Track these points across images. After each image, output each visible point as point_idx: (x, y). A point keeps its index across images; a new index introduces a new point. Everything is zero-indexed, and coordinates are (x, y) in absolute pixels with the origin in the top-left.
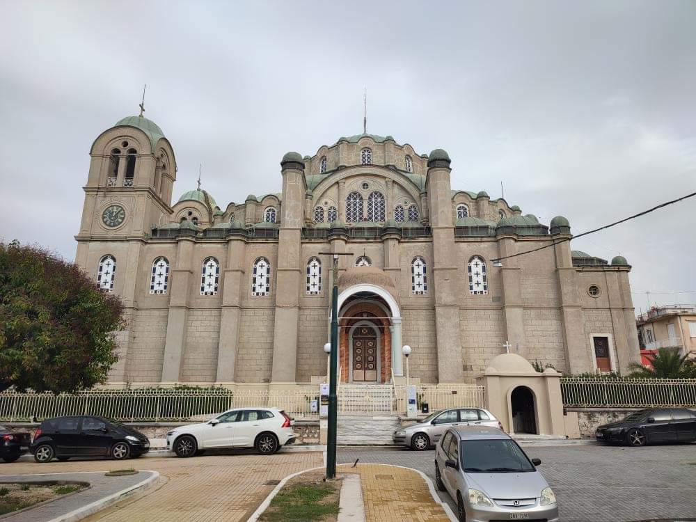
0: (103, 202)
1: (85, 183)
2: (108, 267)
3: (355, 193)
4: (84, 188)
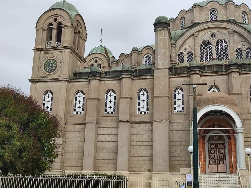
0: (44, 57)
3: (206, 41)
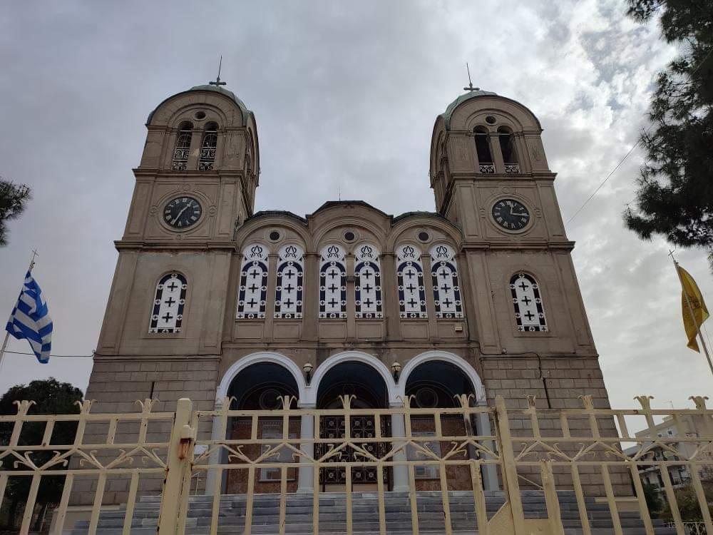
1: (137, 165)
2: (172, 292)
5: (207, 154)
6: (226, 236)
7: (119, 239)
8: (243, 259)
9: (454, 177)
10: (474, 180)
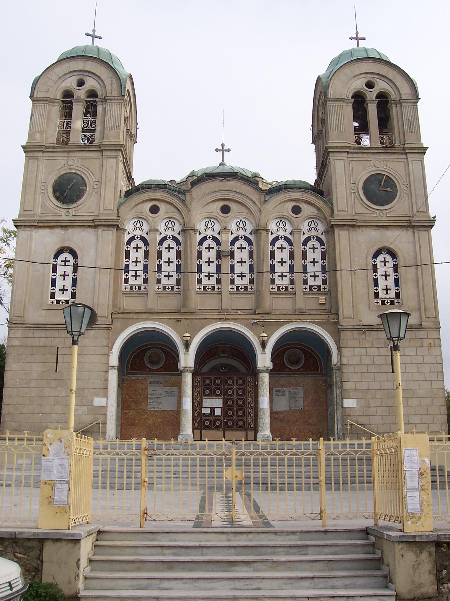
4: (23, 147)
5: (88, 124)
6: (111, 212)
7: (16, 217)
8: (270, 233)
9: (329, 150)
10: (348, 152)
